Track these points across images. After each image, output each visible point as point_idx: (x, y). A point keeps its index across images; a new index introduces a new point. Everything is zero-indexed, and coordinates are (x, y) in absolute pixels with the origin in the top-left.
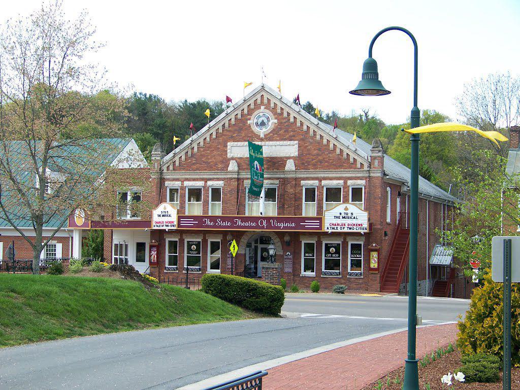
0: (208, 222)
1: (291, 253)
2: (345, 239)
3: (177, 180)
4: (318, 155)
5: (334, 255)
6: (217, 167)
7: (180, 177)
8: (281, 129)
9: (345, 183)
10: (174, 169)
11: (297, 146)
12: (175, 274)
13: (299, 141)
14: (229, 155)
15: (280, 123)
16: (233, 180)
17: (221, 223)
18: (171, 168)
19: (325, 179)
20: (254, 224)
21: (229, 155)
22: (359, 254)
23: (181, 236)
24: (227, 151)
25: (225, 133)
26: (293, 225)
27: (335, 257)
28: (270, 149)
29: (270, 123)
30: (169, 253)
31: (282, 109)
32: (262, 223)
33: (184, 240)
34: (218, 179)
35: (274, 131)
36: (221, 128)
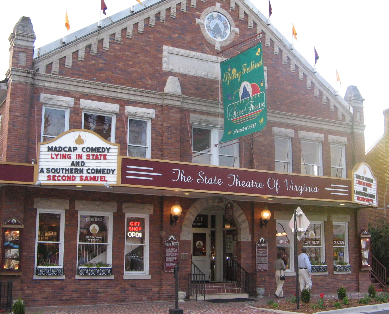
0: (181, 176)
3: (66, 93)
7: (72, 88)
10: (60, 73)
12: (56, 282)
14: (165, 67)
15: (242, 34)
16: (174, 110)
17: (237, 182)
18: (56, 68)
19: (134, 103)
23: (72, 204)
24: (161, 59)
25: (159, 28)
32: (272, 184)
36: (153, 18)
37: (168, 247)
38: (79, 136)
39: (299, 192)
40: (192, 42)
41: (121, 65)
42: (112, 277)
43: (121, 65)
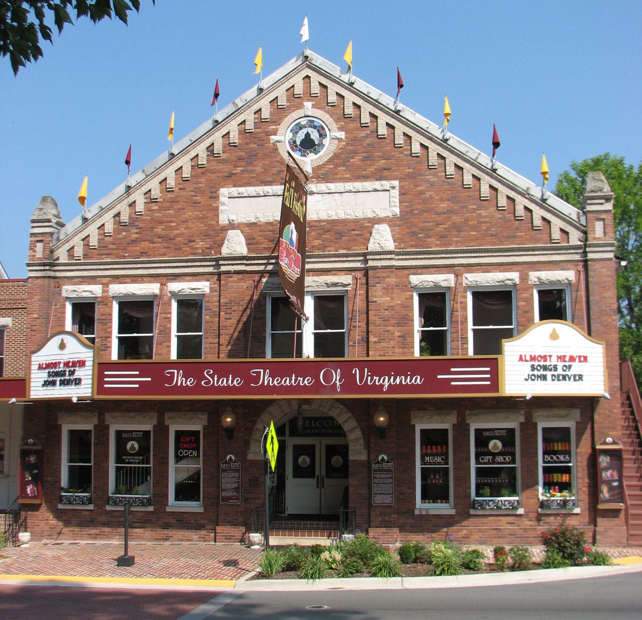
1: (236, 456)
2: (529, 417)
3: (92, 280)
4: (450, 212)
5: (500, 459)
6: (192, 248)
8: (355, 153)
9: (524, 278)
11: (396, 193)
12: (84, 513)
13: (401, 180)
15: (352, 140)
17: (215, 381)
19: (470, 268)
20: (307, 382)
21: (223, 219)
22: (194, 449)
25: (215, 166)
26: (418, 380)
27: (502, 462)
28: (324, 204)
29: (326, 142)
30: (448, 468)
31: (357, 107)
32: (328, 377)
33: (108, 427)
34: (195, 276)
35: (335, 159)
37: (224, 471)
38: (554, 330)
39: (382, 386)
40: (266, 171)
41: (159, 230)
42: (151, 509)
43: (159, 230)
